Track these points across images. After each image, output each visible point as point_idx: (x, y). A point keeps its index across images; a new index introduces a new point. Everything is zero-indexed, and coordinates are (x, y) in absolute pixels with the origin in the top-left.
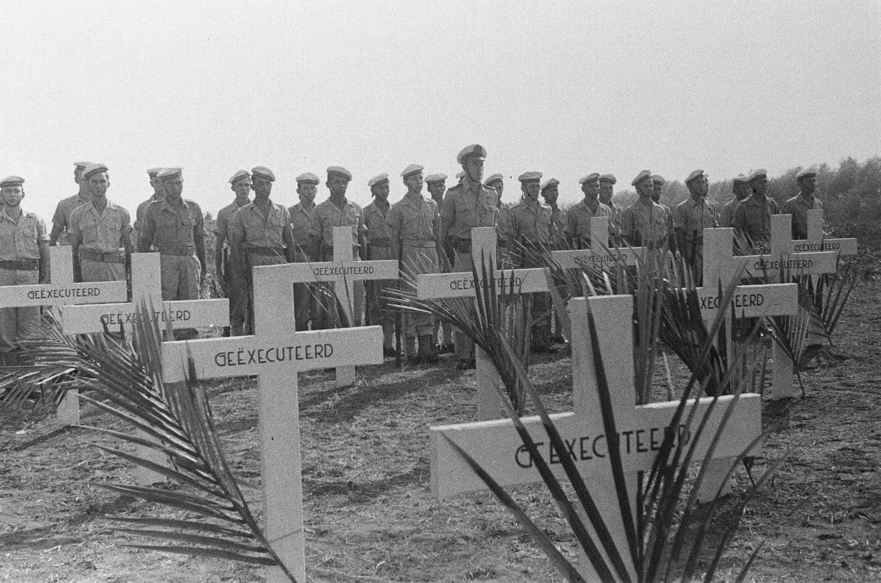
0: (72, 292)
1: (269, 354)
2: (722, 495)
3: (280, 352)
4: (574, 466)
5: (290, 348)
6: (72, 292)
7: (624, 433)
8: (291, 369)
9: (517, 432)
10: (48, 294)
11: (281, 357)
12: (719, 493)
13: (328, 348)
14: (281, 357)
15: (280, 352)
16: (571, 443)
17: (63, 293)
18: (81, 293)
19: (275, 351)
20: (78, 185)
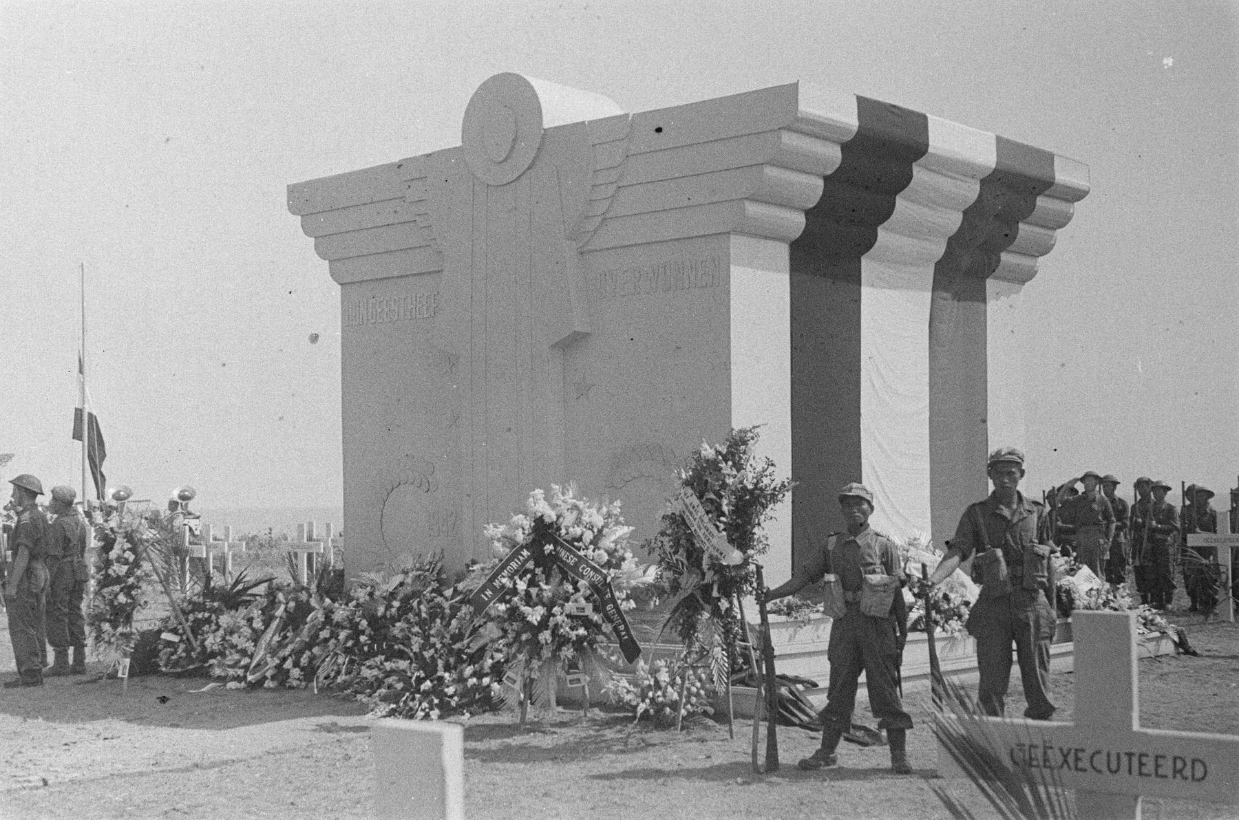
0: (1125, 759)
1: (1095, 759)
2: (1185, 489)
3: (1113, 759)
4: (838, 742)
5: (1130, 755)
6: (1125, 759)
7: (1126, 754)
8: (1219, 535)
9: (994, 142)
10: (1060, 759)
11: (1114, 766)
12: (1183, 491)
13: (1199, 767)
14: (1114, 766)
15: (1113, 759)
16: (1065, 766)
17: (1100, 761)
18: (1149, 767)
19: (1104, 756)
20: (828, 701)
